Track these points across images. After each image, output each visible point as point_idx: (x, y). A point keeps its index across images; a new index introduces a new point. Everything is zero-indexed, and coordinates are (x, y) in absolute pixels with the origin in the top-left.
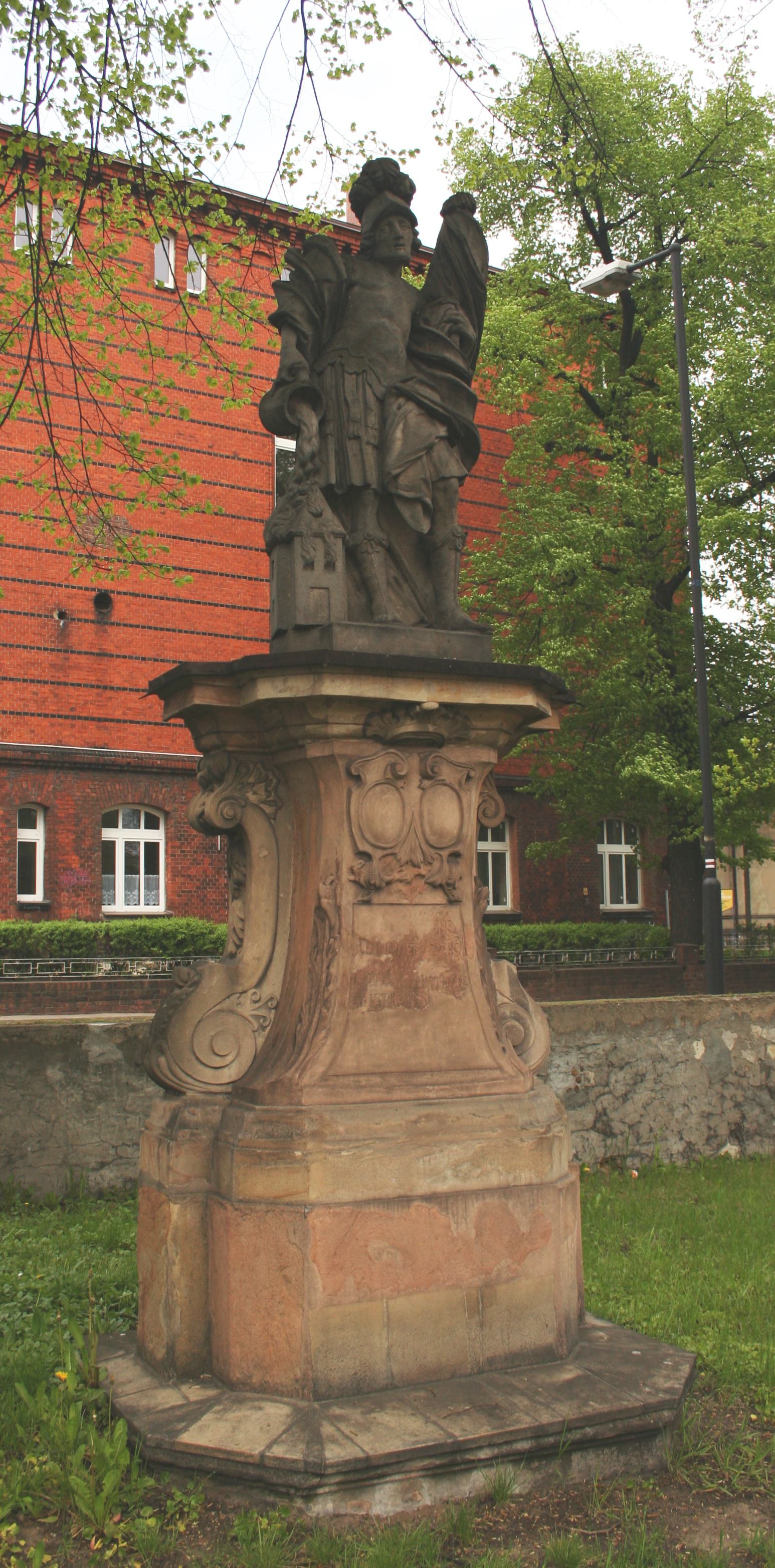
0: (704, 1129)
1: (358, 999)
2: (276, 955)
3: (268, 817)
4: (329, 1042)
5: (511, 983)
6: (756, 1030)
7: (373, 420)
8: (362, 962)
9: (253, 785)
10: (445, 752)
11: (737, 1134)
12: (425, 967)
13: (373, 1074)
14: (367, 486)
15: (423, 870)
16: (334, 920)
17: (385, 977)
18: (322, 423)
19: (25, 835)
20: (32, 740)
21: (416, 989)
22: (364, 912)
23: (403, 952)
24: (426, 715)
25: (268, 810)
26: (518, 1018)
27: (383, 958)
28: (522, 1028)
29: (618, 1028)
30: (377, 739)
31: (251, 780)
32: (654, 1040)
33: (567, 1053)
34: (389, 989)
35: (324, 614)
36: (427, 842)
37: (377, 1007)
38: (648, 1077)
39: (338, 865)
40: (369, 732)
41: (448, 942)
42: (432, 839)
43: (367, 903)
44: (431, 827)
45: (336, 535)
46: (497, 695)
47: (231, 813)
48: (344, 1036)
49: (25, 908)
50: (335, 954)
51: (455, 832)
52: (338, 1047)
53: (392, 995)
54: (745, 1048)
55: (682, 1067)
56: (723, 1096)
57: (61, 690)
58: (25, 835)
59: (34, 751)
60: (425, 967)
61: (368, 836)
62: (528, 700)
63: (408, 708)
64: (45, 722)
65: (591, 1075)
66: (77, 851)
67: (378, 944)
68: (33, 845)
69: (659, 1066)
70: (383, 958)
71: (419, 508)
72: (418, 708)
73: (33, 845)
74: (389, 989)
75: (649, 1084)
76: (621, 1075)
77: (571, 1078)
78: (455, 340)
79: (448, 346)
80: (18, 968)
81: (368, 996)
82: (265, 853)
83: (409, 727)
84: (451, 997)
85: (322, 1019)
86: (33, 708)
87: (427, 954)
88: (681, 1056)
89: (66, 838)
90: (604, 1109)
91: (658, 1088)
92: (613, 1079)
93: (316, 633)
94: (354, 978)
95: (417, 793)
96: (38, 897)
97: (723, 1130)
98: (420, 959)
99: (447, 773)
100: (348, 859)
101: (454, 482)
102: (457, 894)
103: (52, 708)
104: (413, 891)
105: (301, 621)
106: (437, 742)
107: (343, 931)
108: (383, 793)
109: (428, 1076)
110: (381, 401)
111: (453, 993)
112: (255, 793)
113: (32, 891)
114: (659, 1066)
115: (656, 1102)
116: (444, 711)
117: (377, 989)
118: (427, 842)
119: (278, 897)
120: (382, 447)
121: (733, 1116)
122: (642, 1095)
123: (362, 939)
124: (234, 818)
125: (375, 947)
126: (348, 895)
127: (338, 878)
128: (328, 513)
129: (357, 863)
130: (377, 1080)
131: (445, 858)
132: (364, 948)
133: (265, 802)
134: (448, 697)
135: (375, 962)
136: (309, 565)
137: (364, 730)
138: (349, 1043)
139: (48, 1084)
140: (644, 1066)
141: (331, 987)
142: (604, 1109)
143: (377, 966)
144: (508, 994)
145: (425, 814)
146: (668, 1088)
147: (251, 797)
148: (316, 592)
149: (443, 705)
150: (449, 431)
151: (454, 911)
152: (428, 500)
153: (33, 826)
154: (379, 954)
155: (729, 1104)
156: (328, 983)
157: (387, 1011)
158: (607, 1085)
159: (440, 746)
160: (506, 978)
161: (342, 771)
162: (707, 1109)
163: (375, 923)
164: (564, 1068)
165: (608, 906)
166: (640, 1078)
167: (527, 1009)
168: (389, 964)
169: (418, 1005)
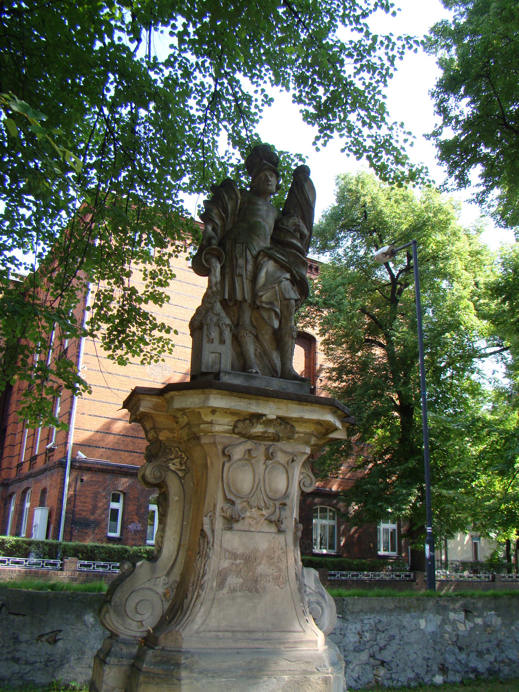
0: (425, 667)
1: (221, 585)
2: (179, 558)
3: (180, 478)
4: (202, 610)
5: (316, 581)
6: (452, 616)
7: (250, 267)
8: (225, 564)
9: (173, 459)
10: (279, 444)
11: (443, 670)
12: (262, 568)
13: (227, 631)
14: (245, 300)
15: (264, 512)
16: (211, 539)
17: (238, 573)
18: (223, 268)
19: (114, 505)
20: (120, 462)
21: (256, 581)
22: (228, 535)
23: (249, 559)
24: (269, 422)
25: (181, 474)
26: (318, 603)
27: (238, 562)
28: (320, 608)
29: (382, 610)
30: (242, 435)
31: (172, 457)
32: (400, 618)
33: (355, 623)
34: (241, 580)
35: (217, 367)
36: (267, 495)
37: (233, 590)
38: (397, 637)
39: (215, 506)
40: (236, 430)
41: (276, 555)
42: (270, 494)
43: (230, 529)
44: (270, 488)
45: (227, 326)
46: (305, 408)
47: (159, 474)
48: (211, 607)
49: (111, 540)
50: (209, 557)
51: (284, 491)
52: (208, 614)
53: (242, 584)
54: (446, 624)
55: (414, 632)
56: (435, 649)
57: (136, 440)
58: (114, 505)
59: (121, 467)
60: (262, 568)
61: (233, 489)
62: (329, 418)
63: (258, 417)
64: (127, 454)
65: (367, 635)
66: (137, 514)
67: (235, 554)
68: (118, 510)
69: (402, 632)
70: (238, 562)
71: (273, 314)
72: (264, 418)
73: (118, 510)
74: (241, 580)
75: (397, 641)
76: (383, 635)
77: (357, 636)
78: (298, 235)
79: (295, 237)
80: (103, 566)
81: (227, 583)
82: (177, 498)
83: (258, 429)
84: (277, 587)
85: (198, 596)
86: (122, 447)
87: (264, 561)
88: (413, 627)
89: (131, 508)
90: (374, 653)
91: (402, 643)
92: (378, 637)
93: (211, 376)
94: (220, 573)
95: (262, 467)
96: (117, 535)
97: (435, 667)
98: (260, 564)
99: (281, 458)
100: (220, 503)
101: (293, 302)
102: (283, 527)
103: (131, 448)
104: (257, 523)
105: (204, 370)
106: (276, 438)
107: (215, 545)
108: (243, 466)
109: (261, 634)
110: (255, 258)
111: (279, 585)
112: (174, 464)
113: (115, 532)
114: (402, 632)
115: (401, 651)
116: (279, 421)
117: (233, 581)
118: (267, 495)
119: (183, 524)
120: (254, 280)
121: (440, 659)
122: (394, 646)
123: (226, 550)
124: (160, 477)
125: (234, 556)
126: (219, 524)
127: (215, 514)
128: (223, 314)
129: (227, 506)
130: (230, 634)
131: (278, 506)
132: (227, 556)
133: (180, 470)
134: (282, 413)
135: (233, 564)
136: (211, 341)
137: (233, 429)
138: (214, 611)
139: (85, 623)
140: (394, 631)
141: (205, 578)
142: (374, 653)
143: (234, 567)
144: (313, 588)
145: (267, 480)
146: (407, 643)
147: (172, 467)
148: (214, 355)
149: (278, 417)
150: (291, 276)
151: (281, 538)
152: (278, 310)
153: (118, 501)
154: (235, 559)
155: (438, 653)
156: (204, 575)
157: (239, 594)
158: (375, 641)
159: (278, 441)
160: (313, 578)
161: (220, 452)
162: (426, 655)
163: (233, 541)
164: (354, 630)
165: (381, 553)
166: (393, 637)
167: (324, 597)
168: (241, 566)
169: (257, 591)
